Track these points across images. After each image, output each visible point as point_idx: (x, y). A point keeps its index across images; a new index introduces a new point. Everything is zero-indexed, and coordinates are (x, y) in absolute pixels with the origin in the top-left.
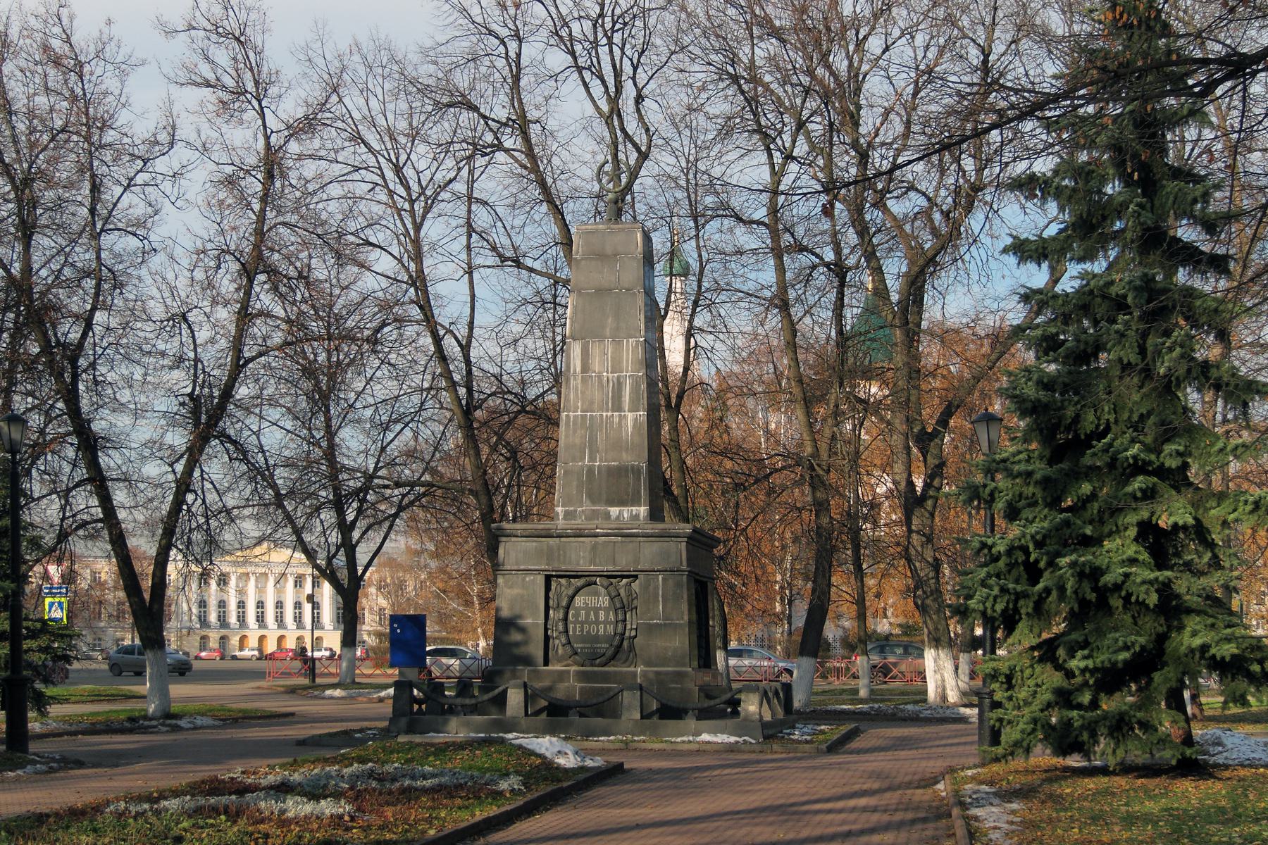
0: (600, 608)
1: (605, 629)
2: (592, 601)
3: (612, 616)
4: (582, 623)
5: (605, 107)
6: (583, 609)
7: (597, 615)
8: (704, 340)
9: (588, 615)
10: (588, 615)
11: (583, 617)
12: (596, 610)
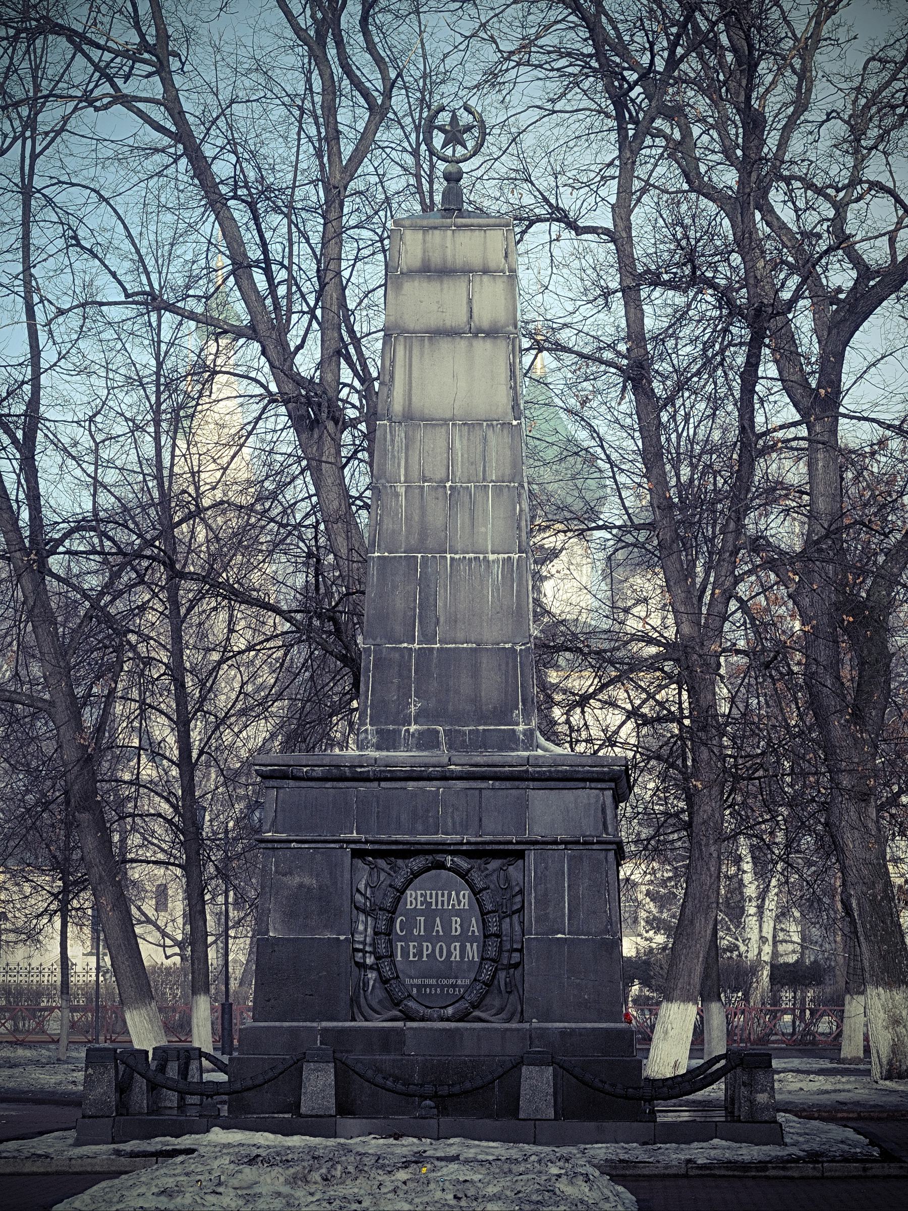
0: (458, 913)
3: (475, 927)
4: (420, 939)
6: (422, 913)
7: (447, 926)
12: (446, 915)
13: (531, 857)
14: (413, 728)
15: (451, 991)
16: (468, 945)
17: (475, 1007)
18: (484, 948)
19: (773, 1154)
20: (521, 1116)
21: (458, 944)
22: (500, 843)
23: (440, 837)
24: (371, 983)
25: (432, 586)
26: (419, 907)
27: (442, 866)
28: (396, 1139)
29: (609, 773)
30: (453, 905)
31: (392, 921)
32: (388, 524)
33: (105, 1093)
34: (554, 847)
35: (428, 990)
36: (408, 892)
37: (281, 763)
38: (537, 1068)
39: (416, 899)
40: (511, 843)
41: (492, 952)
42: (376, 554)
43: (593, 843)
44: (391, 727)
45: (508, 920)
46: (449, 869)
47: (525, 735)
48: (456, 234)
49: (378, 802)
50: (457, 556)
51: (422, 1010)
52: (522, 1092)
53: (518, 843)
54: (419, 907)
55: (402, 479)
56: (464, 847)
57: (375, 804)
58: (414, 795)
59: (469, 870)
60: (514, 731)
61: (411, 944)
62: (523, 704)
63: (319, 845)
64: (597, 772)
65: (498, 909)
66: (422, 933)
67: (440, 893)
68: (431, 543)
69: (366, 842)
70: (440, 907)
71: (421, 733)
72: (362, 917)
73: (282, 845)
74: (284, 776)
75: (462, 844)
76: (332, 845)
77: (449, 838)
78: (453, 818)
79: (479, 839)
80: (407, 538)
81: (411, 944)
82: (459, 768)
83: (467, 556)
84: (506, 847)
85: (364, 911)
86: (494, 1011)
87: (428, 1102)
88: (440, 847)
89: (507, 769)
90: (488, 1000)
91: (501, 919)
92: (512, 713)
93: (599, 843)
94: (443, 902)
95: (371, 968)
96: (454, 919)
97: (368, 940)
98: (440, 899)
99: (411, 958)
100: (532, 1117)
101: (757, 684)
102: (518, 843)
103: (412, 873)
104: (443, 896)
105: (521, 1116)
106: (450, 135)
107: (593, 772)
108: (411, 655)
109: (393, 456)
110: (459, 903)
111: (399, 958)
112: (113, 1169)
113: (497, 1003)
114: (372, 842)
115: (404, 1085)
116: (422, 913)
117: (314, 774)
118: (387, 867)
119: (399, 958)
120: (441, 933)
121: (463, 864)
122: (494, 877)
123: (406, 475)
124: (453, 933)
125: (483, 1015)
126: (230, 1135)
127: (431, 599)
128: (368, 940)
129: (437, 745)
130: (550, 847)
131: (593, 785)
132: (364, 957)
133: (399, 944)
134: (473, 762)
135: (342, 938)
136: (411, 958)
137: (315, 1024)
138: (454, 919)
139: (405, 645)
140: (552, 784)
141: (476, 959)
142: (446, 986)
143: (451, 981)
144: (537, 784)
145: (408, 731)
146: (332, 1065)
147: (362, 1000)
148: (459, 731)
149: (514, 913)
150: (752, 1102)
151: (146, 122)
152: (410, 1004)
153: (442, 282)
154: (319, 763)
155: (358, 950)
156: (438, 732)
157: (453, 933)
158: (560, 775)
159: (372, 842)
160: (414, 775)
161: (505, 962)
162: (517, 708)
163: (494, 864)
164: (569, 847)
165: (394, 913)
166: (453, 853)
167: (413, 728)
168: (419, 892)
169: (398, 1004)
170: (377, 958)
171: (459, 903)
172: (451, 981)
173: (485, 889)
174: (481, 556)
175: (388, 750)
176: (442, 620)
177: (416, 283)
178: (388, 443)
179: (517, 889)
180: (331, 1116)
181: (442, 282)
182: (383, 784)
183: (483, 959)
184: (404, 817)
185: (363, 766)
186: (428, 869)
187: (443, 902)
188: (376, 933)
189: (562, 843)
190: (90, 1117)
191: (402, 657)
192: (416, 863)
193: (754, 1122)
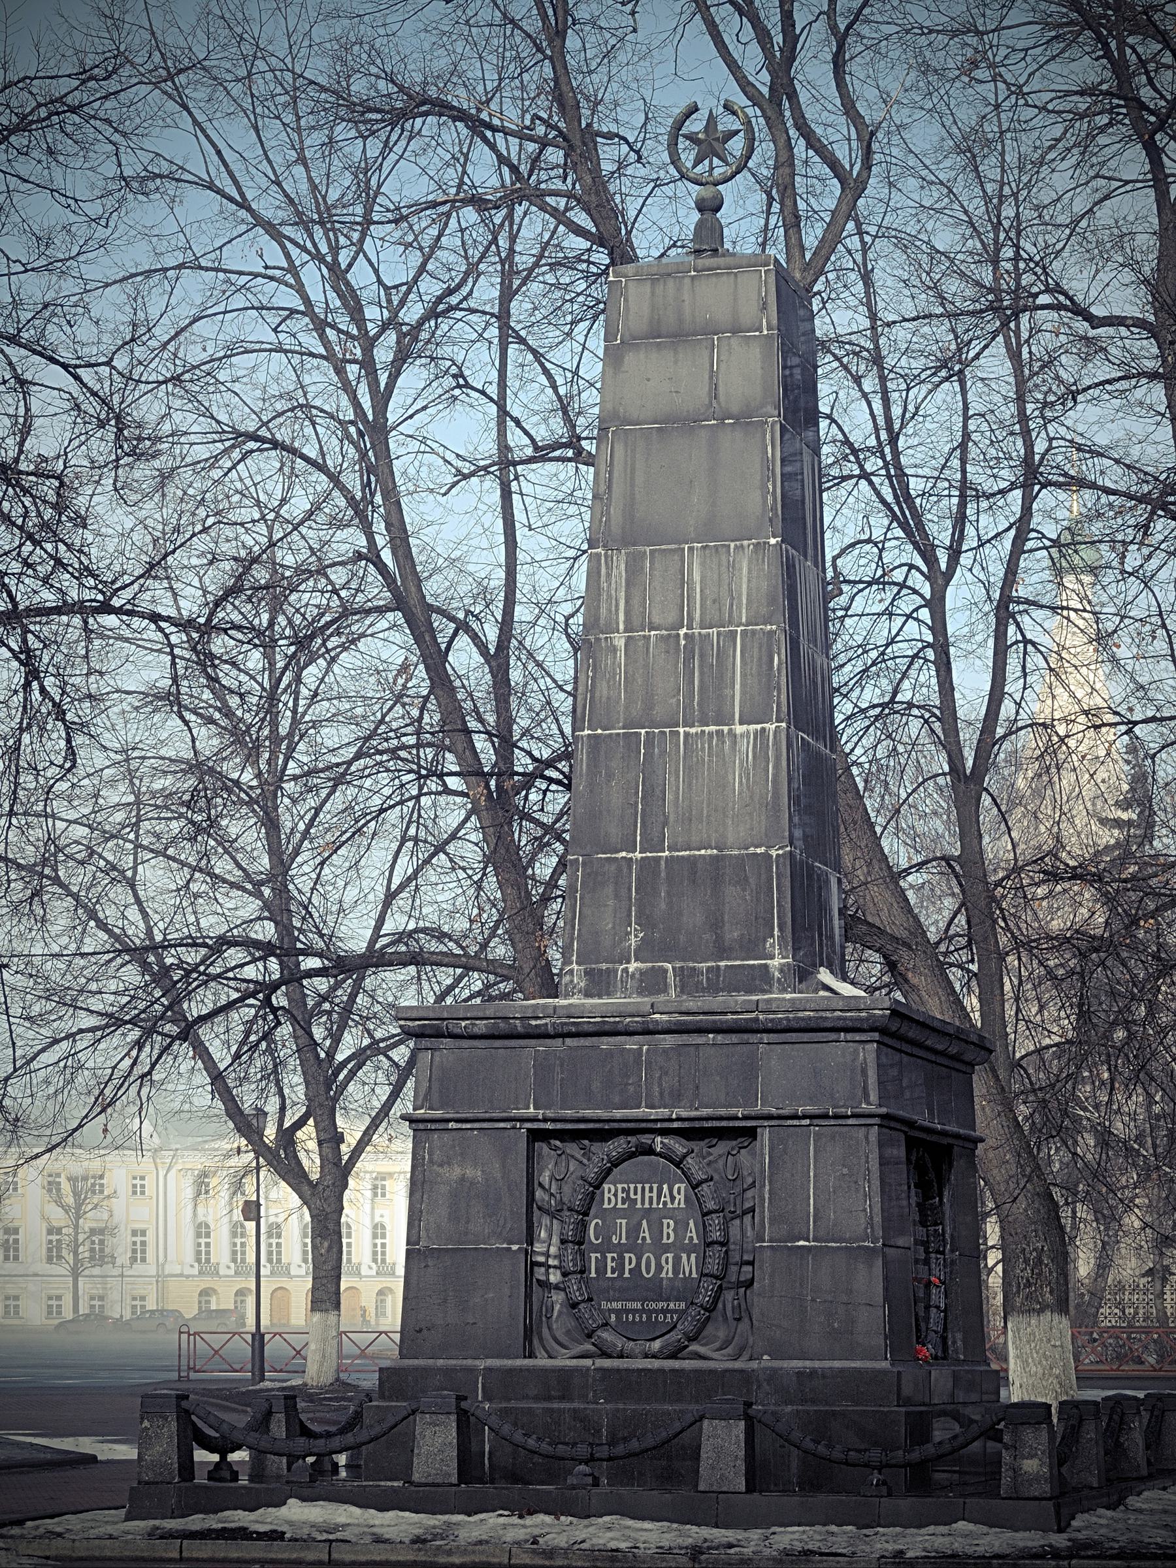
0: (667, 1213)
1: (677, 1261)
2: (646, 1195)
3: (692, 1233)
4: (621, 1249)
5: (762, 81)
6: (623, 1214)
7: (657, 1232)
8: (1035, 624)
9: (634, 1231)
10: (634, 1231)
11: (620, 1237)
12: (654, 1217)
13: (765, 1136)
14: (633, 966)
15: (661, 1318)
16: (684, 1256)
17: (692, 1339)
18: (702, 1262)
19: (1021, 1544)
20: (701, 1488)
21: (670, 1256)
22: (721, 1118)
23: (643, 1111)
24: (557, 1307)
25: (660, 772)
26: (619, 1206)
27: (650, 1151)
28: (521, 1517)
29: (867, 1019)
30: (665, 1203)
31: (584, 1226)
32: (603, 690)
33: (165, 1452)
34: (796, 1122)
35: (630, 1317)
36: (606, 1186)
37: (432, 1015)
38: (723, 1423)
39: (615, 1195)
40: (736, 1118)
41: (713, 1266)
42: (586, 732)
43: (848, 1117)
44: (604, 966)
45: (737, 1222)
46: (660, 1155)
47: (781, 971)
48: (697, 283)
49: (562, 1065)
50: (693, 730)
51: (619, 1343)
52: (703, 1455)
53: (745, 1118)
54: (619, 1206)
55: (621, 627)
56: (675, 1125)
57: (558, 1069)
58: (610, 1054)
59: (685, 1156)
60: (766, 966)
61: (609, 1256)
62: (780, 929)
63: (485, 1125)
64: (851, 1019)
65: (722, 1210)
66: (624, 1241)
67: (647, 1186)
68: (659, 712)
69: (545, 1120)
70: (647, 1206)
71: (642, 973)
72: (546, 1220)
73: (437, 1126)
74: (439, 1035)
75: (671, 1120)
76: (502, 1125)
77: (653, 1113)
78: (660, 1085)
79: (694, 1114)
80: (627, 707)
81: (609, 1256)
82: (665, 1017)
83: (707, 729)
84: (731, 1124)
85: (547, 1212)
86: (717, 1345)
87: (582, 1467)
88: (644, 1125)
89: (730, 1017)
90: (709, 1330)
91: (726, 1223)
92: (765, 941)
93: (854, 1116)
94: (651, 1198)
95: (557, 1287)
96: (665, 1221)
97: (553, 1250)
98: (647, 1194)
99: (609, 1275)
100: (715, 1488)
101: (25, 814)
102: (745, 1118)
103: (609, 1161)
104: (651, 1190)
105: (701, 1488)
106: (703, 146)
107: (845, 1019)
108: (630, 869)
109: (609, 596)
110: (673, 1198)
111: (593, 1275)
112: (127, 1553)
113: (722, 1334)
114: (554, 1120)
115: (550, 1444)
116: (623, 1214)
117: (476, 1030)
118: (578, 1154)
119: (593, 1275)
120: (648, 1241)
121: (679, 1146)
122: (721, 1163)
123: (626, 621)
124: (665, 1241)
125: (702, 1350)
126: (306, 1510)
127: (658, 792)
128: (553, 1250)
129: (665, 990)
130: (790, 1122)
131: (850, 1036)
132: (547, 1274)
133: (593, 1255)
134: (683, 1009)
135: (515, 1247)
136: (609, 1275)
137: (477, 1362)
138: (665, 1221)
139: (624, 854)
140: (793, 1037)
141: (694, 1275)
142: (656, 1311)
143: (661, 1305)
144: (773, 1037)
145: (626, 970)
146: (453, 1417)
147: (545, 1331)
148: (694, 969)
149: (744, 1213)
150: (1016, 1471)
151: (1111, 317)
152: (605, 1335)
153: (676, 352)
154: (480, 1015)
155: (540, 1264)
156: (666, 971)
157: (665, 1241)
158: (802, 1024)
159: (554, 1120)
160: (607, 1028)
161: (734, 1279)
162: (772, 936)
163: (722, 1147)
164: (816, 1122)
165: (586, 1214)
166: (664, 1132)
167: (633, 966)
168: (620, 1186)
169: (589, 1336)
170: (564, 1275)
171: (673, 1198)
172: (661, 1305)
173: (706, 1181)
174: (726, 729)
175: (600, 997)
176: (672, 818)
177: (642, 356)
178: (603, 579)
179: (750, 1180)
180: (452, 1485)
181: (676, 352)
182: (568, 1041)
183: (702, 1275)
184: (596, 1085)
185: (538, 1018)
186: (632, 1155)
187: (651, 1198)
188: (563, 1242)
189: (804, 1117)
190: (147, 1483)
191: (620, 870)
192: (616, 1147)
193: (1018, 1499)
